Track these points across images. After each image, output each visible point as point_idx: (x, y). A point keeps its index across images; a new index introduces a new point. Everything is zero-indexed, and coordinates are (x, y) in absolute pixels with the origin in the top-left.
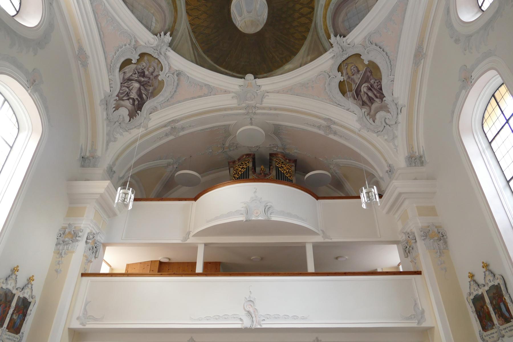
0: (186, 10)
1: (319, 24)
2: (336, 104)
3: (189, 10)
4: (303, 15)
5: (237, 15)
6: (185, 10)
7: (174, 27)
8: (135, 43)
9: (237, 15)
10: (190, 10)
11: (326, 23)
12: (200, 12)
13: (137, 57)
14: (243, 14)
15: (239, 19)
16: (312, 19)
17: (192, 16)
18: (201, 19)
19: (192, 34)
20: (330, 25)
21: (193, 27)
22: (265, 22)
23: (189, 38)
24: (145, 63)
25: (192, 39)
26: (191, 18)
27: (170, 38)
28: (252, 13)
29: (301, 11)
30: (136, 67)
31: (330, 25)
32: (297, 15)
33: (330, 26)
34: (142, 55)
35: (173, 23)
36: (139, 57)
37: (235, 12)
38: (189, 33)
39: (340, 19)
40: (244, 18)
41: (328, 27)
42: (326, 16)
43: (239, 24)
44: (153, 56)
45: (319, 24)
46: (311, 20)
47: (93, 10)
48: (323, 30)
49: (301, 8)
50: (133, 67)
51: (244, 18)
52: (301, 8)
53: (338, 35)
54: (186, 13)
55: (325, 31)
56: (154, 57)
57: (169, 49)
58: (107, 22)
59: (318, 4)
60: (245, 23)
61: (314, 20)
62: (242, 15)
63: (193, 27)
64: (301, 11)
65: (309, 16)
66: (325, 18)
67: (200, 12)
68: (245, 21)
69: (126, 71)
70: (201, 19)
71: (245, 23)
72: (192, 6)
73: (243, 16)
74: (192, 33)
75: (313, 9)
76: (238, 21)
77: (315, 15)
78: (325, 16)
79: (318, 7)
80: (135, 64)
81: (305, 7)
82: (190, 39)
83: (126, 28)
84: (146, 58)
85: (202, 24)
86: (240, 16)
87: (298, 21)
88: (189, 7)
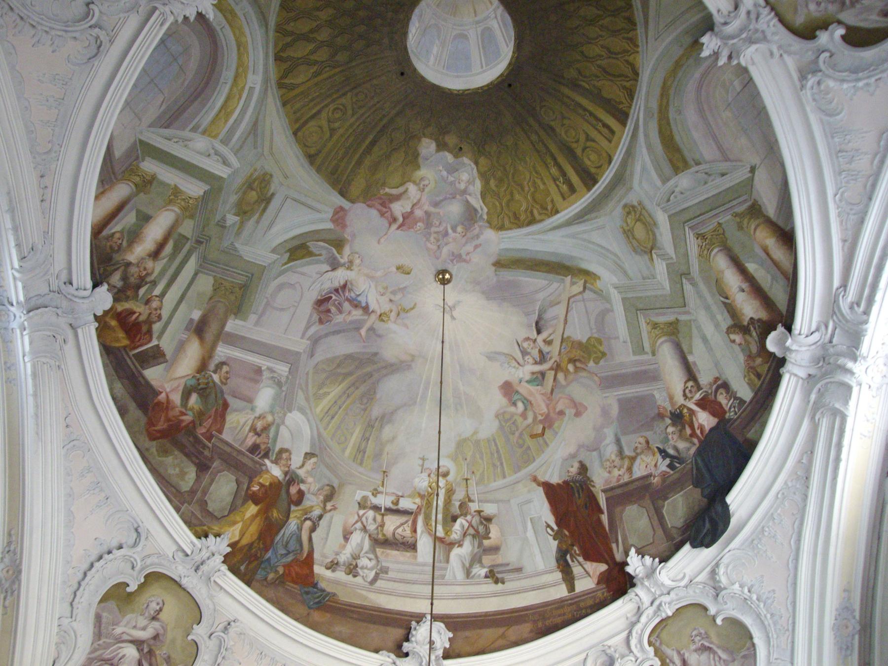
0: (637, 80)
1: (257, 27)
2: (263, 108)
3: (629, 77)
4: (305, 37)
5: (498, 33)
6: (640, 80)
7: (683, 55)
8: (810, 76)
9: (498, 33)
10: (627, 77)
11: (235, 35)
12: (599, 62)
13: (823, 38)
14: (479, 33)
15: (494, 24)
16: (279, 34)
17: (627, 61)
18: (602, 46)
19: (639, 17)
20: (223, 33)
21: (630, 35)
22: (417, 11)
23: (652, 13)
24: (809, 10)
25: (643, 7)
26: (631, 59)
27: (705, 39)
28: (453, 34)
29: (311, 46)
30: (841, 11)
31: (223, 33)
32: (324, 35)
33: (221, 29)
34: (807, 33)
35: (683, 65)
36: (818, 33)
37: (502, 45)
38: (646, 23)
39: (196, 53)
40: (478, 22)
41: (227, 26)
42: (239, 49)
43: (495, 10)
44: (777, 15)
45: (255, 24)
46: (280, 30)
47: (870, 199)
48: (240, 14)
49: (313, 52)
50: (850, 17)
51: (478, 22)
52: (313, 52)
53: (192, 19)
54: (640, 72)
55: (236, 14)
56: (773, 14)
57: (718, 19)
58: (853, 157)
59: (266, 71)
60: (475, 12)
61: (271, 34)
62: (483, 33)
63: (630, 35)
64: (311, 46)
65: (289, 39)
66: (241, 46)
67: (599, 62)
68: (476, 16)
69: (878, 15)
70: (602, 46)
71: (475, 12)
72: (618, 83)
73: (479, 30)
74: (637, 20)
75: (278, 58)
76: (496, 17)
77: (271, 46)
78: (242, 49)
79: (266, 65)
80: (839, 22)
81: (301, 58)
82: (648, 8)
83: (813, 119)
84: (799, 20)
85: (604, 34)
86: (489, 29)
87: (318, 22)
88: (628, 84)
